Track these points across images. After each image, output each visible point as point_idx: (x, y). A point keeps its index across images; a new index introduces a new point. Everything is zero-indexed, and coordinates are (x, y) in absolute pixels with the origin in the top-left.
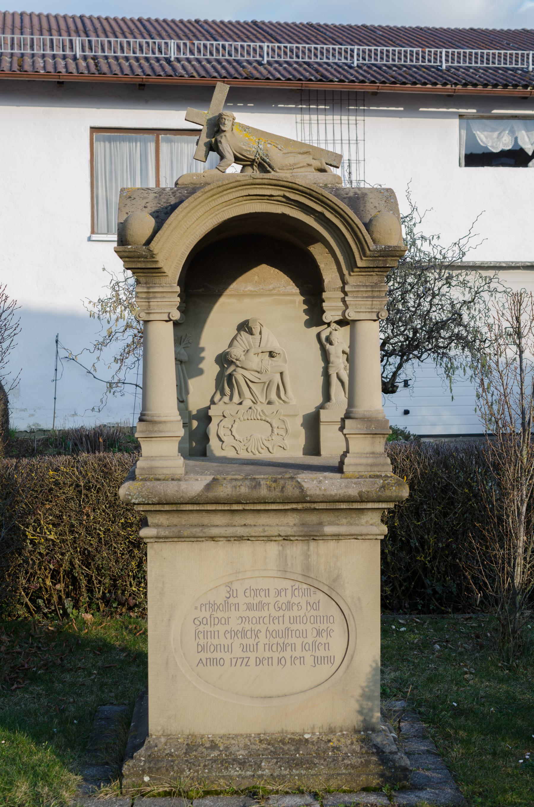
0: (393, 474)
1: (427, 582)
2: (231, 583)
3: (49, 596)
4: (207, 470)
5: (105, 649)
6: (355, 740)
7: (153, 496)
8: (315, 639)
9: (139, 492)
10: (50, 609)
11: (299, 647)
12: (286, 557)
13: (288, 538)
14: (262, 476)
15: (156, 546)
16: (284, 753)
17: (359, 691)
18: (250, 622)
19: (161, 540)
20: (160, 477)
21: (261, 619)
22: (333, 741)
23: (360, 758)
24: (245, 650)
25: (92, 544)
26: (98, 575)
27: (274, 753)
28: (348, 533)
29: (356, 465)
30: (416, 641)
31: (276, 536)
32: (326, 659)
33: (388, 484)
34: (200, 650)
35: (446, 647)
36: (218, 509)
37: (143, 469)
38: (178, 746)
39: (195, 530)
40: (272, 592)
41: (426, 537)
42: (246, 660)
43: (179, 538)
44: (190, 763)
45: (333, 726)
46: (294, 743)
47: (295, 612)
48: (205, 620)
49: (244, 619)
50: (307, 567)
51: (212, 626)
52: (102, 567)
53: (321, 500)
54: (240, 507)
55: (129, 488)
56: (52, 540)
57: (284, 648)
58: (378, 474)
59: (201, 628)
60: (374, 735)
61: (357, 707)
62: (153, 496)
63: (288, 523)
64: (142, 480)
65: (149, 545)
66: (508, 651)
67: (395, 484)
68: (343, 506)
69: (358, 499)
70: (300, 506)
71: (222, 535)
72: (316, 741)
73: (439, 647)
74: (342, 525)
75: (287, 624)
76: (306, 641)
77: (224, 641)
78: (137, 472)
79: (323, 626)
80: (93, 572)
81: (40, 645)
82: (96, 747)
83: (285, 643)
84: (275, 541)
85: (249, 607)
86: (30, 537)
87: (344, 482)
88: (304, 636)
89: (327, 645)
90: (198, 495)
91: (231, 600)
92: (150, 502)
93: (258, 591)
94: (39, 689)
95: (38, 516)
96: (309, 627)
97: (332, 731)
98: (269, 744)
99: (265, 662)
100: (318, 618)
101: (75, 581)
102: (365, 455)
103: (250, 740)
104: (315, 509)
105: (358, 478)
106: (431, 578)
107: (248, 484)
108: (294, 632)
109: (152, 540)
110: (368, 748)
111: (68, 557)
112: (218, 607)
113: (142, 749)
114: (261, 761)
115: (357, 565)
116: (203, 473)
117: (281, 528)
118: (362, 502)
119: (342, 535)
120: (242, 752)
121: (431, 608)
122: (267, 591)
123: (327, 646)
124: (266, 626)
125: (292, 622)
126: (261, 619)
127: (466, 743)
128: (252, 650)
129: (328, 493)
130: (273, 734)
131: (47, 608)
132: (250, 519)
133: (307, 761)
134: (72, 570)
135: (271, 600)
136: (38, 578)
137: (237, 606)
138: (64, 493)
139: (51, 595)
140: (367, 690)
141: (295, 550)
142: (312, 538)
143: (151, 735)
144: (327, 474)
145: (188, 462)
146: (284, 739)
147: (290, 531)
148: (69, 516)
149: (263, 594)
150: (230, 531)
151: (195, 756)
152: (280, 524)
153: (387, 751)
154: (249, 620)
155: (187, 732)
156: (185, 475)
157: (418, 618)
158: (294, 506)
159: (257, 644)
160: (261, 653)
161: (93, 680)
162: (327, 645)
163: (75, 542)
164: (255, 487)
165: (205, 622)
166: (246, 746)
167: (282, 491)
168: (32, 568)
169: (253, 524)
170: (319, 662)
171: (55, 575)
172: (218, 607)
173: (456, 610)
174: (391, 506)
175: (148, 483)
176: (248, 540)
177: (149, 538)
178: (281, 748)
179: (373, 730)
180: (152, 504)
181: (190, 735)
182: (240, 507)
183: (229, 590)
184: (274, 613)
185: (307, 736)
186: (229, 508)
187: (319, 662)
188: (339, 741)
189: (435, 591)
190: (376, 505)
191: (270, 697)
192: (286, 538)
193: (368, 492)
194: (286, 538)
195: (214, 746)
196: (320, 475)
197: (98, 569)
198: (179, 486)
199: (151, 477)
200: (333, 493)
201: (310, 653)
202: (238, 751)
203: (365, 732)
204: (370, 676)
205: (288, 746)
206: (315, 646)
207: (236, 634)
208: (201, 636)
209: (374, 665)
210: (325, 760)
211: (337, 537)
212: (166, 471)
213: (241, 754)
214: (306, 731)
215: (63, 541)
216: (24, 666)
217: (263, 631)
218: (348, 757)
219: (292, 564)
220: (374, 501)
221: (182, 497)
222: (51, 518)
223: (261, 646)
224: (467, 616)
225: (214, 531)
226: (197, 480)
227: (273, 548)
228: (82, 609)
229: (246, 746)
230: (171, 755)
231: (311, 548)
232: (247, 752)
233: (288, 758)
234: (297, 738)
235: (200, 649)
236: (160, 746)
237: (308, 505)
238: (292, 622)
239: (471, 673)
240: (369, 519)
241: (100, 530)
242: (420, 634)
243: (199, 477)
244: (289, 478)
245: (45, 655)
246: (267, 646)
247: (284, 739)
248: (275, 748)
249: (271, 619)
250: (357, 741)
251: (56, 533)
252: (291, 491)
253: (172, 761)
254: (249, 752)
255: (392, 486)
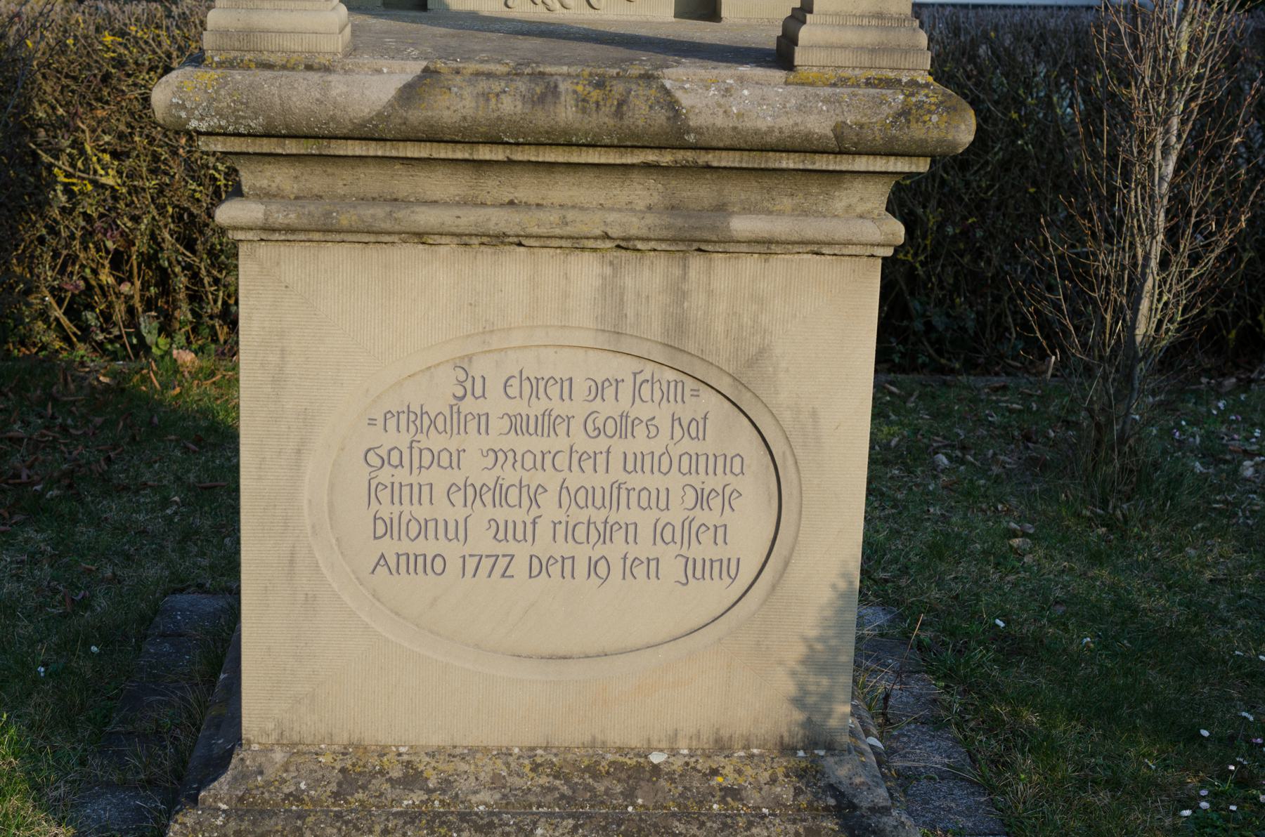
0: (930, 79)
1: (915, 305)
2: (470, 358)
3: (108, 307)
4: (412, 44)
5: (212, 440)
6: (780, 772)
7: (249, 113)
8: (692, 514)
9: (211, 100)
10: (110, 333)
11: (645, 533)
12: (622, 294)
13: (630, 244)
14: (565, 69)
15: (263, 251)
16: (595, 800)
17: (800, 650)
18: (518, 465)
19: (276, 236)
20: (272, 59)
21: (548, 458)
22: (723, 772)
23: (794, 822)
24: (501, 535)
25: (198, 200)
26: (213, 265)
27: (570, 800)
28: (795, 238)
29: (830, 47)
30: (893, 443)
31: (596, 238)
32: (716, 565)
33: (920, 105)
34: (380, 532)
35: (963, 462)
36: (435, 155)
37: (224, 33)
38: (319, 775)
39: (371, 211)
40: (581, 388)
41: (920, 211)
42: (503, 562)
43: (327, 231)
44: (346, 823)
45: (725, 733)
46: (623, 776)
47: (640, 443)
48: (395, 454)
49: (500, 455)
50: (678, 326)
51: (415, 471)
52: (221, 251)
53: (728, 143)
54: (499, 154)
55: (180, 88)
56: (112, 187)
57: (606, 536)
58: (891, 75)
59: (385, 475)
60: (831, 760)
61: (790, 688)
62: (249, 113)
63: (632, 203)
64: (220, 65)
65: (243, 250)
66: (1104, 481)
67: (938, 106)
68: (788, 162)
69: (833, 144)
70: (666, 158)
71: (446, 229)
72: (679, 770)
73: (945, 460)
74: (781, 213)
75: (617, 473)
76: (665, 517)
77: (443, 511)
78: (208, 41)
79: (712, 483)
80: (201, 260)
81: (69, 421)
82: (130, 728)
83: (611, 522)
84: (594, 250)
85: (517, 425)
86: (62, 178)
87: (795, 95)
88: (662, 505)
89: (720, 531)
90: (379, 114)
91: (468, 405)
92: (242, 130)
93: (542, 384)
94: (37, 537)
95: (79, 134)
96: (675, 481)
97: (722, 746)
98: (556, 777)
99: (555, 569)
100: (702, 460)
101: (164, 278)
102: (858, 22)
103: (508, 765)
104: (708, 167)
105: (834, 85)
106: (925, 299)
107: (523, 89)
108: (634, 495)
109: (250, 235)
110: (815, 794)
111: (146, 226)
112: (433, 422)
113: (222, 779)
114: (535, 823)
115: (813, 325)
116: (398, 51)
117: (612, 217)
118: (842, 152)
119: (777, 243)
120: (485, 796)
121: (920, 361)
122: (566, 384)
123: (720, 532)
124: (560, 477)
125: (630, 467)
126: (548, 458)
127: (1045, 748)
128: (520, 536)
129: (749, 124)
130: (568, 749)
131: (103, 330)
132: (526, 188)
133: (655, 825)
134: (156, 252)
135: (577, 408)
136: (83, 266)
137: (483, 421)
138: (135, 85)
139: (110, 306)
140: (819, 647)
141: (648, 278)
142: (695, 246)
143: (249, 742)
144: (745, 70)
145: (360, 19)
146: (597, 763)
147: (635, 226)
148: (147, 136)
149: (554, 391)
150: (468, 219)
151: (362, 803)
152: (609, 204)
153: (865, 804)
154: (515, 458)
155: (342, 738)
156: (346, 56)
157: (891, 383)
158: (651, 157)
159: (534, 523)
160: (544, 546)
161: (169, 520)
162: (720, 531)
163: (161, 192)
164: (542, 99)
165: (395, 459)
166: (496, 777)
167: (619, 112)
168: (68, 246)
169: (533, 199)
170: (699, 574)
171: (118, 261)
172: (433, 422)
173: (971, 366)
174: (922, 166)
175: (237, 75)
176: (520, 244)
177: (242, 229)
178: (588, 788)
179: (830, 747)
180: (249, 135)
181: (351, 744)
182: (499, 154)
183: (462, 376)
184: (583, 443)
185: (656, 758)
186: (467, 156)
187: (699, 574)
188: (739, 772)
189: (929, 326)
190: (879, 164)
191: (565, 658)
192: (625, 244)
193: (861, 126)
194: (625, 244)
195: (412, 778)
196: (728, 73)
197: (212, 253)
198: (326, 87)
199: (248, 56)
200: (762, 125)
201: (674, 549)
202: (475, 792)
203: (809, 752)
204: (828, 613)
205: (606, 783)
206: (691, 533)
207: (478, 494)
208: (385, 495)
209: (842, 585)
210: (702, 824)
211: (766, 246)
212: (290, 43)
213: (483, 800)
214: (655, 744)
215: (134, 190)
216: (19, 477)
217: (553, 487)
218: (764, 817)
219: (637, 315)
220: (874, 153)
221: (333, 118)
222: (107, 138)
223: (544, 528)
224: (997, 381)
225: (426, 218)
226: (379, 71)
227: (586, 272)
228: (180, 338)
229: (496, 777)
230: (296, 797)
231: (692, 274)
232: (498, 796)
233: (606, 817)
234: (631, 762)
235: (380, 532)
236: (270, 773)
237: (690, 155)
238: (630, 467)
239: (1025, 535)
240: (854, 200)
241: (215, 168)
242: (901, 424)
243: (385, 64)
244: (641, 77)
245: (76, 448)
246: (561, 529)
247: (597, 763)
248: (573, 788)
249: (575, 457)
250: (787, 776)
251: (120, 173)
252: (644, 113)
253: (301, 816)
254: (504, 796)
255: (929, 112)
